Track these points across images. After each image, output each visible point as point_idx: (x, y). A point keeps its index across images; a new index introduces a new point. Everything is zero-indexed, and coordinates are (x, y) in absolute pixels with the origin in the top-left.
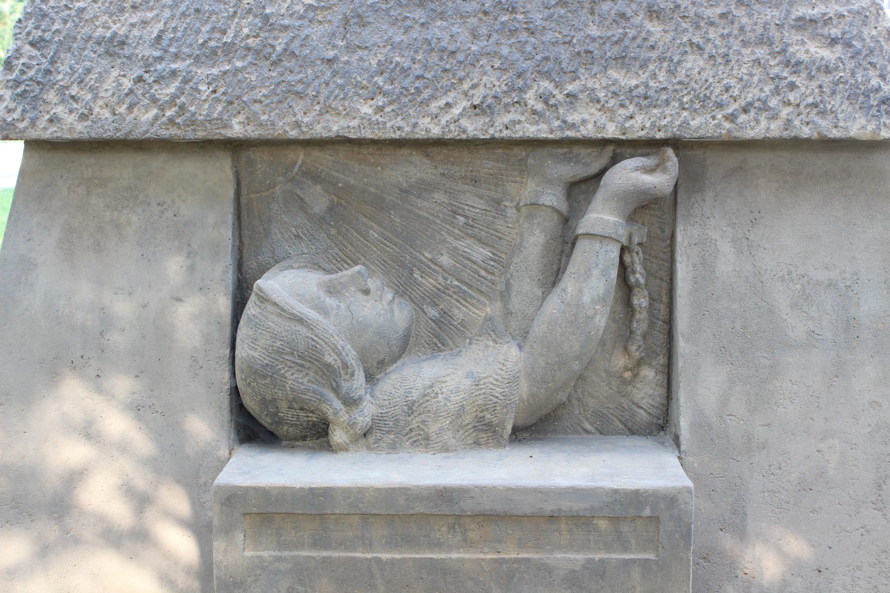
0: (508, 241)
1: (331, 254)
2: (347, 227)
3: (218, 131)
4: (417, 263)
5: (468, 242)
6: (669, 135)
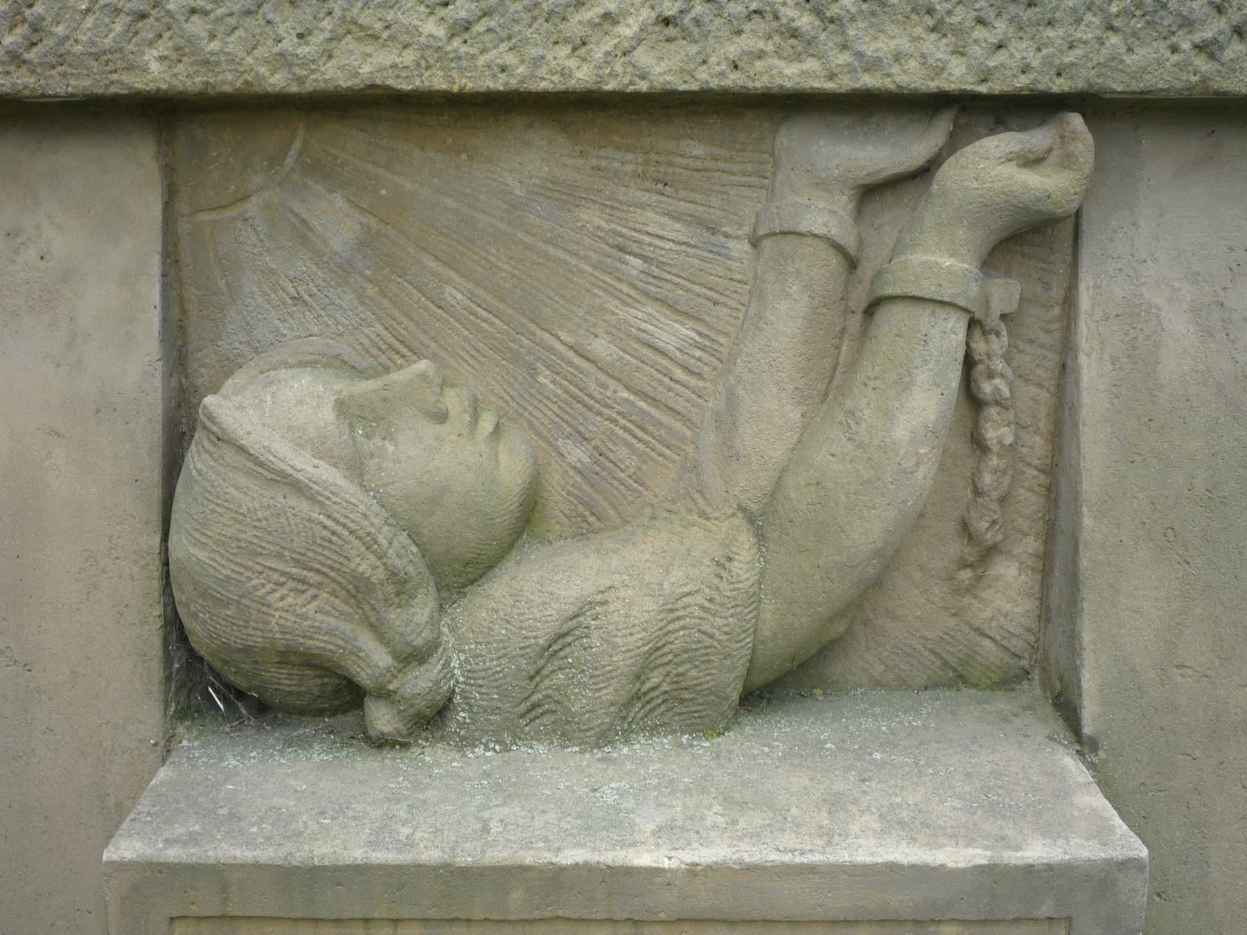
0: (731, 308)
1: (368, 337)
2: (400, 280)
3: (115, 77)
4: (543, 354)
5: (649, 310)
6: (1080, 85)
